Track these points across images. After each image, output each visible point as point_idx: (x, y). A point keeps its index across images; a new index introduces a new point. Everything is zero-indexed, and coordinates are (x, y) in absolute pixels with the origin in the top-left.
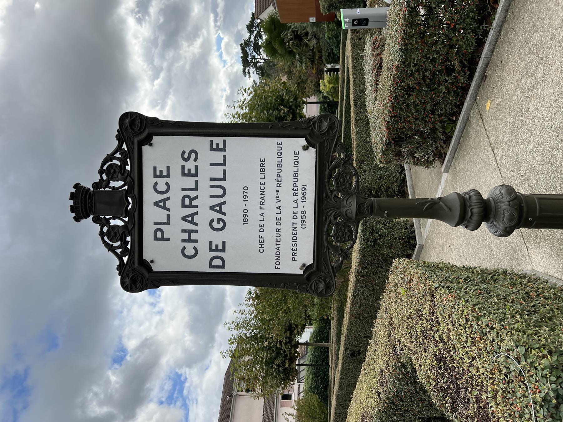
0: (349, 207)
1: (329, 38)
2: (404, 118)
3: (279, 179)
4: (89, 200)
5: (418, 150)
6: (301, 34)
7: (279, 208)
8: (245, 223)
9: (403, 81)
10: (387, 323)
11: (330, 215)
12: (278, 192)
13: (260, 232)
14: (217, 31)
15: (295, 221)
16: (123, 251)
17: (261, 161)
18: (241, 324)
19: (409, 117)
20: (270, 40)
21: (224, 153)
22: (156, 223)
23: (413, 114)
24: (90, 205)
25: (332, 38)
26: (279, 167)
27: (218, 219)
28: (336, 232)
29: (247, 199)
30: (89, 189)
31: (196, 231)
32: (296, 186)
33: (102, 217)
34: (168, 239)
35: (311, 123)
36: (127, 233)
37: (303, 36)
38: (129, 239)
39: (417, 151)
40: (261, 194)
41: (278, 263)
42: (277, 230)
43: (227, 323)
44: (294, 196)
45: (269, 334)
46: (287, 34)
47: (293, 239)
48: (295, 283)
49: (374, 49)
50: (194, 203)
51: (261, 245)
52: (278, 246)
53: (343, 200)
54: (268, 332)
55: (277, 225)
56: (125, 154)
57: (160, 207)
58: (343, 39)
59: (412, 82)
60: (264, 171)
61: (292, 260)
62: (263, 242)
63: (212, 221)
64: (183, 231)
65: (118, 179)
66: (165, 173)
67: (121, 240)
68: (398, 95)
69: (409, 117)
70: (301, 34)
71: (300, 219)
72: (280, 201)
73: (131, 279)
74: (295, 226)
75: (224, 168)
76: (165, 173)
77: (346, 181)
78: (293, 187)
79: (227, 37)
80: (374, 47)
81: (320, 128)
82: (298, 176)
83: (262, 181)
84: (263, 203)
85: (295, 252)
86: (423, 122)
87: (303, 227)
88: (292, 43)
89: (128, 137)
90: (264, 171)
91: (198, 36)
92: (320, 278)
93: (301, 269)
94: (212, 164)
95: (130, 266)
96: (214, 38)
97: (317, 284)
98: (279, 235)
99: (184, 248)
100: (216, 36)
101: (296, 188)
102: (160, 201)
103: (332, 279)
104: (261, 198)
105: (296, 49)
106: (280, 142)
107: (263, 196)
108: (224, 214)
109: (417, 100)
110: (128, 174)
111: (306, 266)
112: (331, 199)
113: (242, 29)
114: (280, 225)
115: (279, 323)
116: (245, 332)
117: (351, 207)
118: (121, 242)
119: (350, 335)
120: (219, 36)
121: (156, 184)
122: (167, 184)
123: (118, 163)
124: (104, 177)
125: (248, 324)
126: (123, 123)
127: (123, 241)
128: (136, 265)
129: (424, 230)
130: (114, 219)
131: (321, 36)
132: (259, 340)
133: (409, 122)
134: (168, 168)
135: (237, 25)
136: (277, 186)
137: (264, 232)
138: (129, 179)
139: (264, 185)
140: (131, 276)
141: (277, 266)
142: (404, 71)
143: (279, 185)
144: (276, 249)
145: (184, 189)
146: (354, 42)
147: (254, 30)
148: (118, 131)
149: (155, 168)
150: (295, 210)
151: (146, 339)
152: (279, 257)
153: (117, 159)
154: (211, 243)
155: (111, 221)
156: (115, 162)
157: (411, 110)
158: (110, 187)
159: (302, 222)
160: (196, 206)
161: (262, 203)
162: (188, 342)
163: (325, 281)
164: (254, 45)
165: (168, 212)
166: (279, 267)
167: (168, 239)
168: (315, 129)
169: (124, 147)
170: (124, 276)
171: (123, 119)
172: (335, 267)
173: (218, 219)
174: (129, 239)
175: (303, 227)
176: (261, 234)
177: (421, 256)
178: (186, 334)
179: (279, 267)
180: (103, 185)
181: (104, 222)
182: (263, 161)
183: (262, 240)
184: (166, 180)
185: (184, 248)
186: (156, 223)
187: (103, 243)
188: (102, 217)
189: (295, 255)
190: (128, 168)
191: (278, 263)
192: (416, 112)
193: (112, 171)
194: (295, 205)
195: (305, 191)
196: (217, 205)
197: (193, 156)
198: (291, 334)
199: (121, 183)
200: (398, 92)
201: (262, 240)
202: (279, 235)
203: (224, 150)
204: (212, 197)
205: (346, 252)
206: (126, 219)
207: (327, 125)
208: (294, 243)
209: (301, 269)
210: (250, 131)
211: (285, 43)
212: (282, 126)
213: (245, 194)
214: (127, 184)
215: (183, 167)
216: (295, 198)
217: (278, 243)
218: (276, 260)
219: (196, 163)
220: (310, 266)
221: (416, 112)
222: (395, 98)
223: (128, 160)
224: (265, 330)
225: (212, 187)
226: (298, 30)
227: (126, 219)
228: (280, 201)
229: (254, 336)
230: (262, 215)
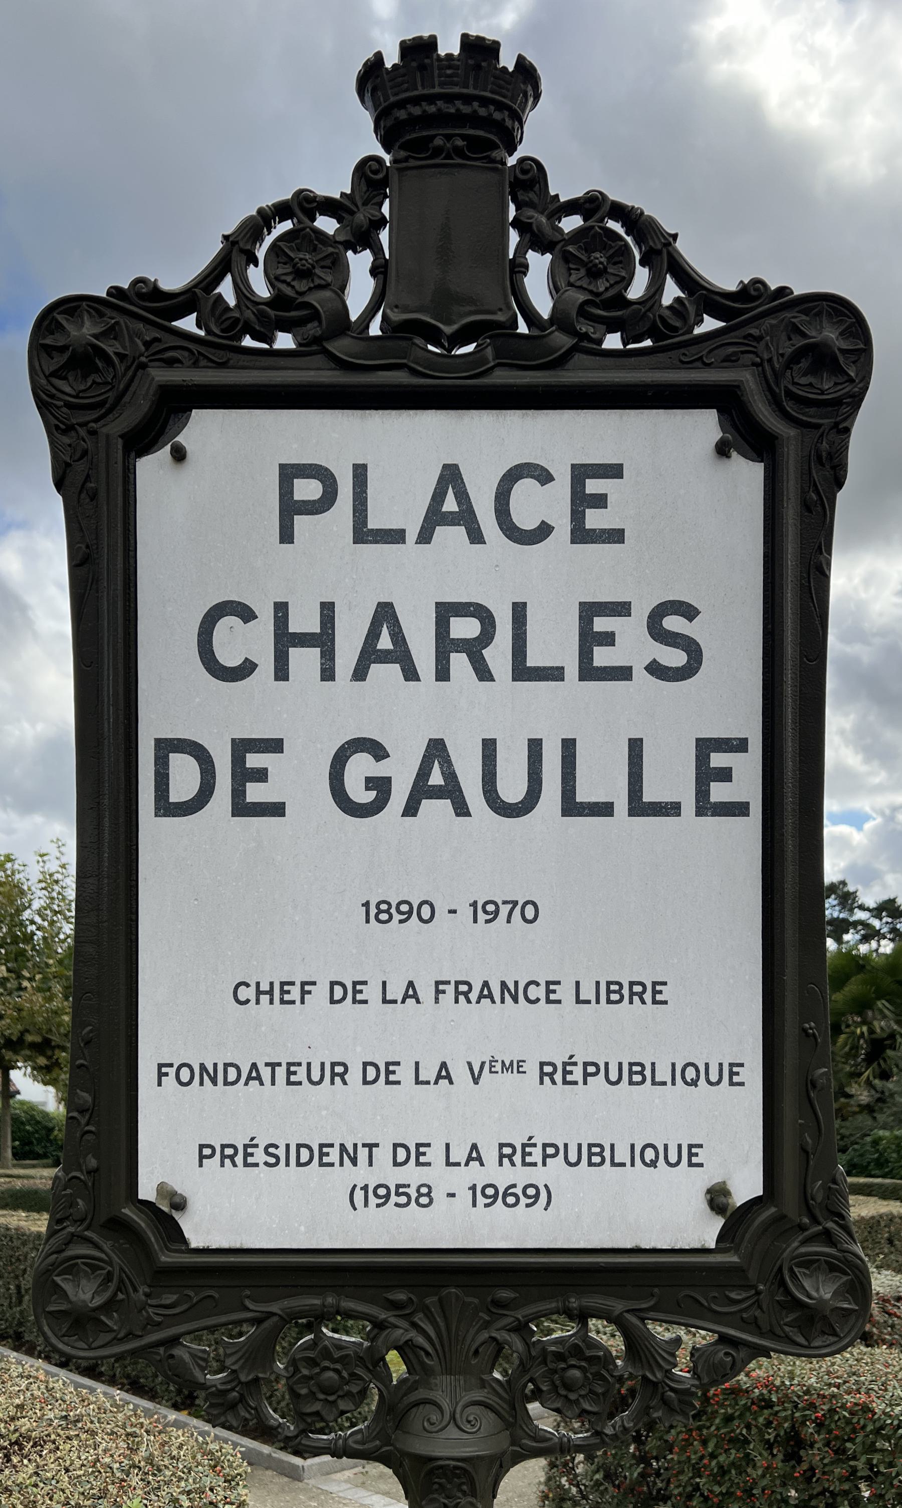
0: (453, 1417)
1: (876, 1142)
2: (700, 1429)
3: (577, 1074)
4: (463, 137)
5: (597, 1471)
6: (885, 1060)
7: (444, 1073)
8: (373, 911)
9: (820, 1425)
10: (25, 1424)
11: (414, 1325)
12: (516, 1067)
13: (333, 984)
14: (882, 813)
15: (383, 1155)
16: (227, 308)
17: (655, 984)
18: (59, 893)
19: (704, 1443)
20: (868, 967)
21: (689, 805)
22: (360, 473)
23: (713, 1456)
24: (438, 142)
25: (877, 1151)
26: (631, 1073)
27: (388, 780)
28: (337, 1355)
29: (482, 916)
30: (512, 150)
31: (328, 674)
32: (545, 1156)
33: (386, 209)
34: (287, 535)
35: (830, 1225)
36: (312, 329)
37: (879, 1065)
38: (284, 341)
39: (594, 1467)
40: (504, 985)
41: (185, 1075)
42: (339, 1069)
43: (62, 849)
44: (502, 1146)
45: (30, 980)
46: (884, 1017)
47: (299, 1146)
48: (93, 1163)
49: (884, 1300)
50: (459, 662)
51: (270, 992)
52: (266, 1073)
53: (483, 1384)
54: (38, 977)
55: (365, 1064)
56: (678, 324)
57: (438, 497)
58: (880, 1185)
59: (814, 1456)
60: (609, 1001)
61: (202, 1147)
62: (282, 1002)
63: (378, 751)
64: (328, 610)
65: (562, 284)
66: (594, 519)
67: (278, 301)
68: (776, 1408)
69: (704, 1443)
70: (885, 1060)
71: (393, 1177)
72: (476, 1081)
73: (94, 346)
74: (363, 1153)
75: (621, 805)
76: (594, 519)
77: (573, 1396)
78: (539, 1140)
79: (865, 841)
80: (888, 1301)
81: (808, 1263)
82: (590, 1164)
83: (565, 993)
84: (466, 994)
85: (239, 1159)
86: (689, 1489)
87: (359, 1195)
88: (862, 1033)
89: (759, 339)
90: (609, 1001)
91: (867, 760)
92: (121, 1281)
93: (163, 1190)
94: (635, 747)
95: (156, 347)
96: (864, 804)
97: (94, 1268)
98: (316, 1077)
99: (246, 614)
100: (867, 809)
101: (536, 1155)
102: (462, 496)
103: (121, 1340)
104: (486, 984)
105: (845, 1044)
106: (744, 1075)
107: (497, 997)
108: (411, 809)
109: (760, 1472)
110: (585, 337)
111: (176, 1215)
112: (487, 1325)
113: (885, 886)
114: (365, 1082)
115: (56, 1013)
116: (36, 905)
117: (452, 1432)
118: (269, 303)
119: (24, 1244)
120: (867, 818)
121: (544, 477)
122: (544, 531)
123: (636, 290)
124: (571, 223)
125: (59, 912)
126: (819, 314)
127: (272, 313)
128: (161, 375)
129: (347, 1481)
130: (374, 272)
131: (881, 1117)
132: (13, 948)
133: (688, 1443)
134: (616, 536)
135: (894, 871)
136: (542, 1064)
137: (333, 1001)
138: (562, 340)
139: (549, 1001)
140: (110, 350)
141: (172, 1071)
142: (854, 1431)
143: (547, 1071)
144: (254, 1066)
145: (519, 612)
146: (883, 1224)
147: (884, 920)
148: (783, 291)
149: (614, 471)
150: (435, 1155)
151: (23, 608)
152: (214, 1082)
153: (656, 288)
154: (275, 746)
155: (366, 257)
156: (641, 278)
157: (726, 1451)
158: (521, 250)
159: (382, 1191)
160: (443, 674)
161: (462, 990)
162: (17, 733)
163: (108, 1306)
164: (845, 921)
165: (412, 535)
166: (169, 1081)
167: (287, 535)
168: (804, 1243)
169: (710, 324)
170: (108, 312)
171: (838, 313)
172: (177, 1352)
173: (388, 780)
174: (284, 341)
175: (359, 1195)
176: (320, 992)
177: (269, 1473)
178: (40, 727)
179: (169, 1081)
180: (531, 212)
181: (362, 217)
182: (655, 992)
183: (295, 993)
184: (563, 526)
185: (246, 614)
186: (360, 473)
187: (260, 211)
188: (386, 209)
189: (223, 1156)
190: (613, 341)
191: (185, 1075)
192: (720, 1467)
193: (599, 257)
194: (459, 1154)
195: (524, 1201)
196: (450, 776)
197: (675, 658)
198: (33, 1046)
199: (543, 305)
200: (785, 1410)
201: (295, 993)
202: (316, 1077)
203: (705, 807)
204: (489, 748)
205: (247, 1406)
206: (375, 329)
207: (821, 1300)
208: (281, 1152)
209: (163, 1190)
210: (790, 934)
211: (859, 1014)
212: (814, 1086)
213: (504, 910)
214: (536, 333)
215: (622, 609)
216: (490, 1154)
217: (281, 1072)
218: (203, 1067)
219: (639, 673)
220: (176, 1234)
221: (720, 1467)
222: (764, 1400)
223: (648, 343)
224: (41, 968)
225: (535, 747)
226: (894, 1049)
227: (375, 329)
228: (476, 1081)
229: (25, 934)
230: (411, 992)
